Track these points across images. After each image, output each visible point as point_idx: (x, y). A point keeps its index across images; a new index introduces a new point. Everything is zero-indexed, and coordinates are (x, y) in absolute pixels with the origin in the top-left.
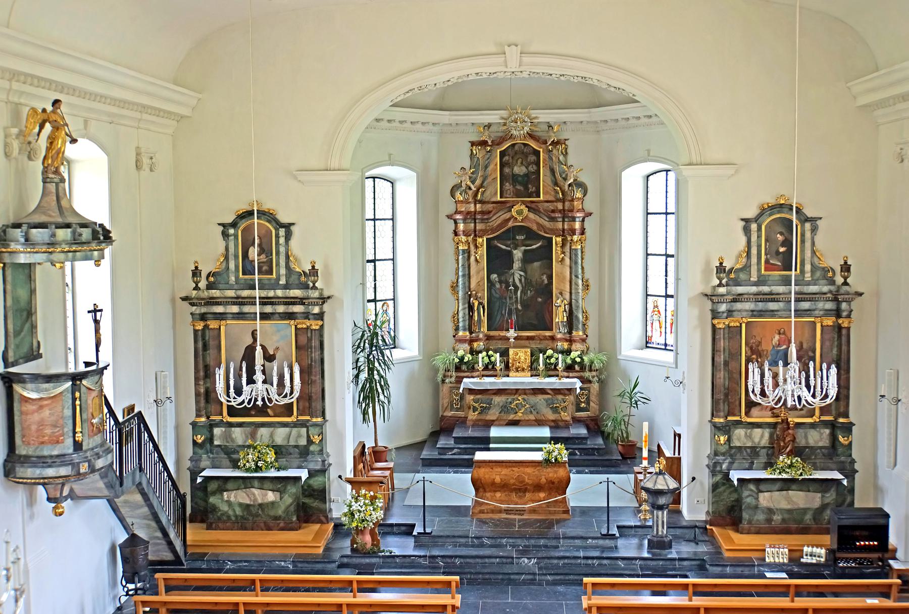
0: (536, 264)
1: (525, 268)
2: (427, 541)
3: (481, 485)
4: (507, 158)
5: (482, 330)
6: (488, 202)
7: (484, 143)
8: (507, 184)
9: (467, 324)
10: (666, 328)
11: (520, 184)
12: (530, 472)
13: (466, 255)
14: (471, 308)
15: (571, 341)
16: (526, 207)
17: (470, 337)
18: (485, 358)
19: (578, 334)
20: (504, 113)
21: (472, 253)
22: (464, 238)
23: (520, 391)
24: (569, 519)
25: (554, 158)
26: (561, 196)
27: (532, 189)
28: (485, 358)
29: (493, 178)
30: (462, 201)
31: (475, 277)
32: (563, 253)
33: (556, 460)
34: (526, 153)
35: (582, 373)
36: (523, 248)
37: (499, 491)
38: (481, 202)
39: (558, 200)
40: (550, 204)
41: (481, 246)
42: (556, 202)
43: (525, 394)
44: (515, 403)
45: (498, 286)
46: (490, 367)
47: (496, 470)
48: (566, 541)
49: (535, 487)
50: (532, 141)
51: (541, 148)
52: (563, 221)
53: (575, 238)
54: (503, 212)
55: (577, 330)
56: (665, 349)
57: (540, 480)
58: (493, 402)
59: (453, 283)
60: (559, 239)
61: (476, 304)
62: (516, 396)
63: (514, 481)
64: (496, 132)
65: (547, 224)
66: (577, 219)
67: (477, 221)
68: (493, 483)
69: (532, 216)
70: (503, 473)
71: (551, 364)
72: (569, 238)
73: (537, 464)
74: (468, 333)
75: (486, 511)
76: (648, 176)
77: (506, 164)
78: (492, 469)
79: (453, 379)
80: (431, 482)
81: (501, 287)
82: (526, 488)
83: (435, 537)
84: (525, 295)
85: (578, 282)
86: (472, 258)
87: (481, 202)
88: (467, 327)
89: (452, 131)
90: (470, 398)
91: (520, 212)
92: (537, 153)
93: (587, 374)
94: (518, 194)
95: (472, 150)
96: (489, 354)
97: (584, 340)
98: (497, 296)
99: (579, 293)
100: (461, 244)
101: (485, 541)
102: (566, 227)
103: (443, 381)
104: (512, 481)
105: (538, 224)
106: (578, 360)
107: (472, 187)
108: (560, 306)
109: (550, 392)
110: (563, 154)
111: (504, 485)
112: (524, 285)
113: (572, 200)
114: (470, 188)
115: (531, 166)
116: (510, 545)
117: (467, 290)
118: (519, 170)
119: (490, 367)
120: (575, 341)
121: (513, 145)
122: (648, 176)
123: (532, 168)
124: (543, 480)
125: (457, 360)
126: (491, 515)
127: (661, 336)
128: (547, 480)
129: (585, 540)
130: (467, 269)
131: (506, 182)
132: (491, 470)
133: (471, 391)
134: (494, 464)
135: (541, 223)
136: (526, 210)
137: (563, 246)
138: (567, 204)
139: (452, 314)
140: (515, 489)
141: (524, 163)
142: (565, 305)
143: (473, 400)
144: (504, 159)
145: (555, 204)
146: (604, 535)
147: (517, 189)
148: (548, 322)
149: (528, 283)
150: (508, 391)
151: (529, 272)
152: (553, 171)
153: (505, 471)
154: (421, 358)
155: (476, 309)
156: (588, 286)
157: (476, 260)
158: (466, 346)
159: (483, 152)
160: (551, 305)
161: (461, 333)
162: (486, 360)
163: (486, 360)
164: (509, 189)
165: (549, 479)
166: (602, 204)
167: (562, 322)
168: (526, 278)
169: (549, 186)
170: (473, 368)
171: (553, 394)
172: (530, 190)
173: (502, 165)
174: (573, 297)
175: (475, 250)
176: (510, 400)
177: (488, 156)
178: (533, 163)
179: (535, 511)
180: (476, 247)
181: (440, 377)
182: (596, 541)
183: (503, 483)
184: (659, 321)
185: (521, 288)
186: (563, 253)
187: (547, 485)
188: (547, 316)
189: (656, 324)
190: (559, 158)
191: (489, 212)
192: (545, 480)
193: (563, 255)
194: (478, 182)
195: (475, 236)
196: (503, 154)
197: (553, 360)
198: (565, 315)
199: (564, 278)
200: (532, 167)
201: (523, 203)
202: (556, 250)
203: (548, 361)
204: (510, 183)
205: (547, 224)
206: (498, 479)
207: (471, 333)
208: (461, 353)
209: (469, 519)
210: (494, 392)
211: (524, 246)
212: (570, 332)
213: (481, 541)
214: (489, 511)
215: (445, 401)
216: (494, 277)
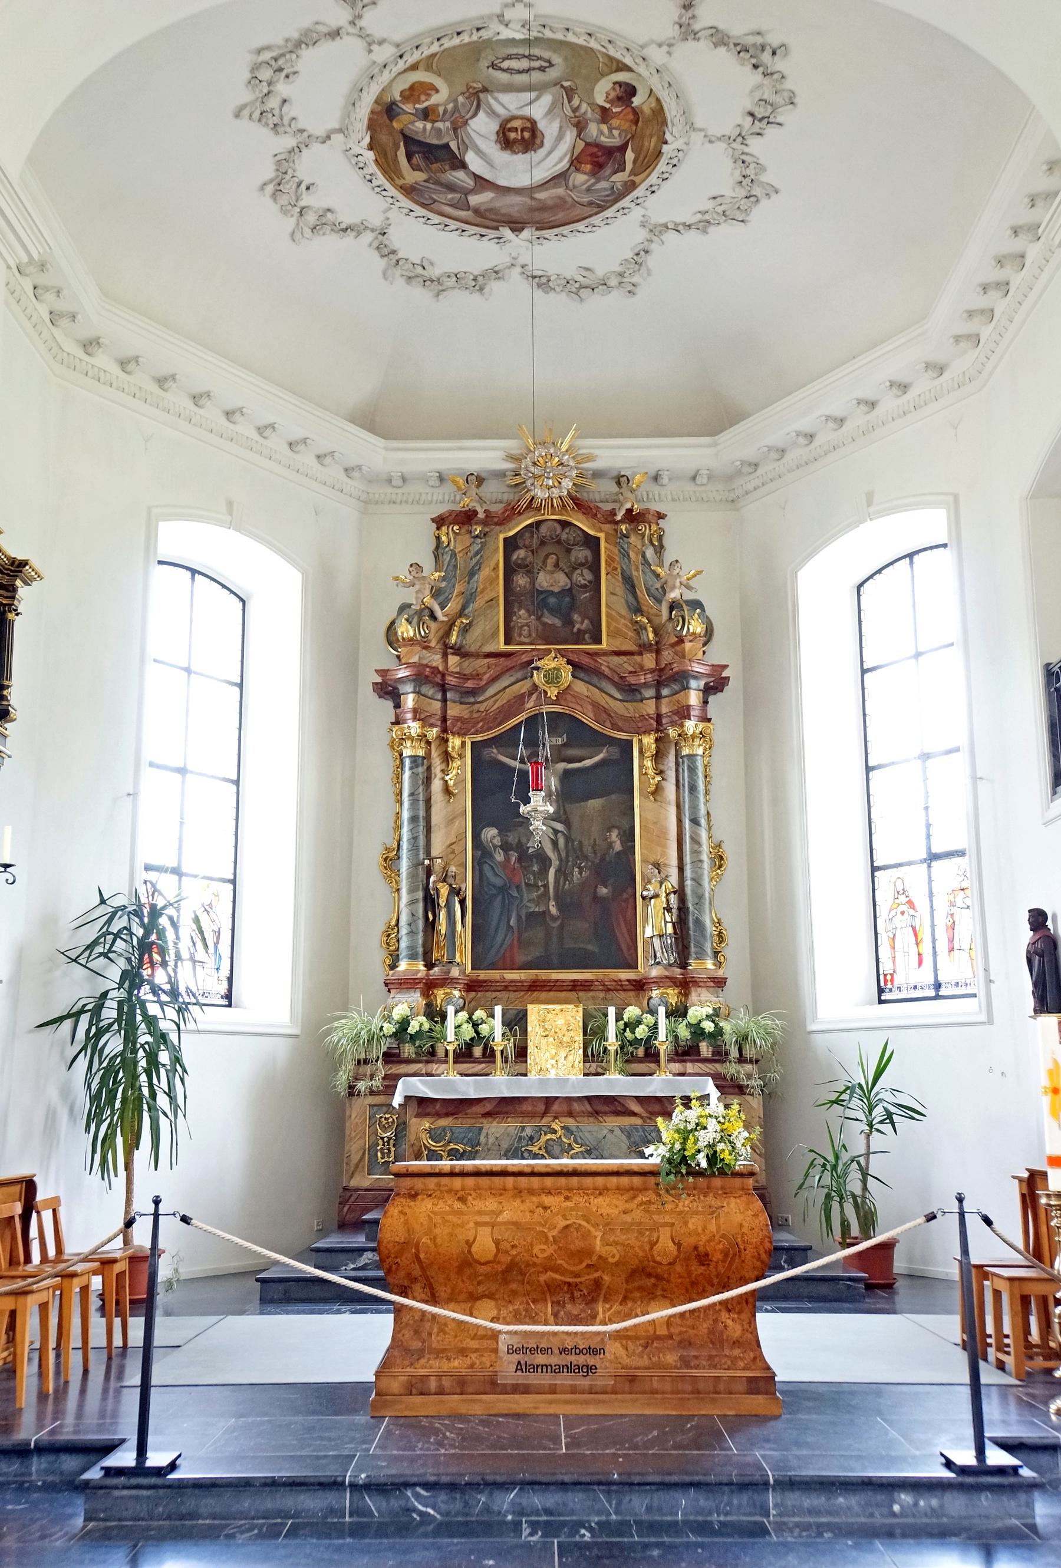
0: (594, 804)
1: (565, 812)
2: (142, 1509)
3: (417, 1272)
4: (521, 553)
5: (458, 959)
6: (477, 655)
7: (466, 518)
8: (522, 612)
9: (420, 941)
10: (934, 941)
11: (553, 612)
12: (613, 1212)
13: (421, 770)
14: (430, 902)
15: (685, 985)
16: (569, 662)
17: (427, 975)
18: (465, 1026)
19: (703, 966)
20: (512, 445)
21: (437, 766)
22: (414, 727)
23: (556, 1107)
24: (776, 1417)
25: (632, 555)
26: (651, 636)
27: (581, 624)
28: (465, 1026)
29: (487, 598)
30: (411, 639)
31: (443, 831)
32: (661, 773)
33: (712, 1159)
34: (567, 541)
35: (718, 1066)
36: (562, 766)
37: (490, 1296)
38: (458, 651)
39: (644, 648)
40: (625, 658)
41: (460, 756)
42: (640, 654)
43: (570, 1114)
44: (544, 1138)
45: (499, 856)
46: (478, 1051)
47: (479, 1205)
48: (794, 1498)
49: (632, 1275)
50: (581, 516)
51: (601, 531)
52: (658, 697)
53: (691, 726)
54: (513, 679)
55: (700, 956)
56: (937, 997)
57: (653, 1244)
58: (482, 1139)
59: (388, 850)
60: (649, 740)
61: (444, 891)
62: (545, 1121)
63: (550, 1250)
64: (495, 493)
65: (618, 707)
66: (693, 683)
67: (449, 695)
68: (466, 1263)
69: (580, 687)
70: (505, 1216)
71: (636, 1042)
72: (672, 732)
73: (637, 1181)
74: (421, 966)
75: (433, 1384)
76: (860, 587)
77: (519, 566)
78: (462, 1200)
79: (377, 1083)
80: (185, 1219)
81: (507, 859)
82: (597, 1283)
83: (182, 1485)
84: (566, 880)
85: (699, 835)
86: (437, 785)
87: (458, 651)
88: (420, 950)
89: (394, 496)
90: (420, 1127)
91: (553, 677)
92: (592, 543)
93: (731, 1069)
94: (549, 636)
95: (438, 538)
96: (474, 1017)
97: (719, 983)
98: (498, 882)
99: (701, 861)
100: (409, 744)
101: (421, 1503)
102: (664, 710)
103: (351, 1089)
104: (541, 1251)
105: (596, 705)
106: (708, 1026)
107: (439, 613)
108: (656, 896)
109: (635, 1107)
110: (653, 545)
111: (511, 1267)
112: (563, 855)
113: (681, 641)
114: (433, 617)
115: (579, 571)
116: (534, 1526)
117: (422, 856)
118: (552, 580)
119: (478, 1051)
120: (696, 983)
121: (539, 523)
122: (860, 587)
123: (583, 577)
124: (666, 1245)
125: (389, 1028)
126: (454, 1401)
127: (920, 963)
128: (679, 1245)
129: (880, 1497)
130: (422, 805)
131: (520, 608)
132: (458, 1205)
133: (422, 1105)
134: (470, 1181)
135: (603, 703)
136: (567, 674)
137: (658, 756)
138: (667, 655)
139: (384, 928)
140: (551, 1288)
141: (561, 564)
142: (667, 895)
143: (430, 1132)
144: (514, 557)
145: (637, 658)
146: (963, 1470)
147: (545, 624)
148: (624, 947)
149: (573, 852)
150: (526, 1107)
151: (575, 820)
152: (629, 583)
153: (512, 1211)
154: (296, 1031)
155: (442, 902)
156: (721, 858)
157: (447, 791)
158: (416, 998)
159: (467, 540)
160: (631, 900)
161: (403, 966)
162: (468, 1032)
163: (468, 1032)
164: (527, 625)
165: (688, 1242)
166: (750, 657)
167: (661, 936)
168: (568, 839)
169: (624, 617)
170: (432, 1053)
171: (644, 1115)
172: (577, 626)
173: (510, 571)
174: (688, 873)
175: (443, 766)
176: (528, 1131)
177: (477, 547)
178: (582, 565)
179: (632, 1379)
180: (447, 757)
181: (343, 1078)
182: (934, 1502)
183: (505, 1259)
184: (914, 929)
185: (555, 863)
186: (661, 773)
187: (679, 1268)
188: (621, 932)
189: (905, 939)
190: (644, 556)
191: (477, 676)
192: (672, 1247)
193: (658, 778)
194: (452, 606)
195: (445, 730)
196: (511, 545)
197: (641, 1032)
198: (668, 919)
199: (663, 833)
200: (582, 575)
201: (562, 653)
202: (641, 766)
203: (628, 1034)
204: (528, 611)
205: (618, 707)
206: (484, 1245)
207: (429, 966)
208: (400, 1011)
209: (362, 1419)
210: (488, 1107)
211: (564, 761)
212: (684, 965)
213: (395, 1503)
214: (446, 1383)
215: (355, 1148)
216: (489, 836)
